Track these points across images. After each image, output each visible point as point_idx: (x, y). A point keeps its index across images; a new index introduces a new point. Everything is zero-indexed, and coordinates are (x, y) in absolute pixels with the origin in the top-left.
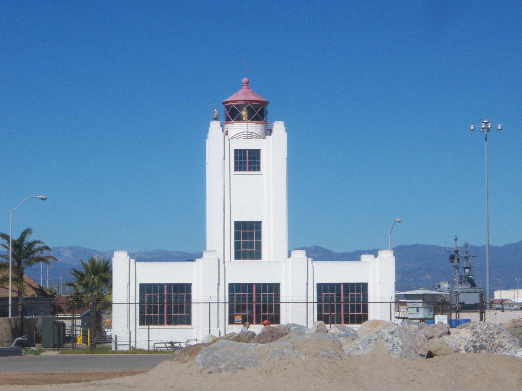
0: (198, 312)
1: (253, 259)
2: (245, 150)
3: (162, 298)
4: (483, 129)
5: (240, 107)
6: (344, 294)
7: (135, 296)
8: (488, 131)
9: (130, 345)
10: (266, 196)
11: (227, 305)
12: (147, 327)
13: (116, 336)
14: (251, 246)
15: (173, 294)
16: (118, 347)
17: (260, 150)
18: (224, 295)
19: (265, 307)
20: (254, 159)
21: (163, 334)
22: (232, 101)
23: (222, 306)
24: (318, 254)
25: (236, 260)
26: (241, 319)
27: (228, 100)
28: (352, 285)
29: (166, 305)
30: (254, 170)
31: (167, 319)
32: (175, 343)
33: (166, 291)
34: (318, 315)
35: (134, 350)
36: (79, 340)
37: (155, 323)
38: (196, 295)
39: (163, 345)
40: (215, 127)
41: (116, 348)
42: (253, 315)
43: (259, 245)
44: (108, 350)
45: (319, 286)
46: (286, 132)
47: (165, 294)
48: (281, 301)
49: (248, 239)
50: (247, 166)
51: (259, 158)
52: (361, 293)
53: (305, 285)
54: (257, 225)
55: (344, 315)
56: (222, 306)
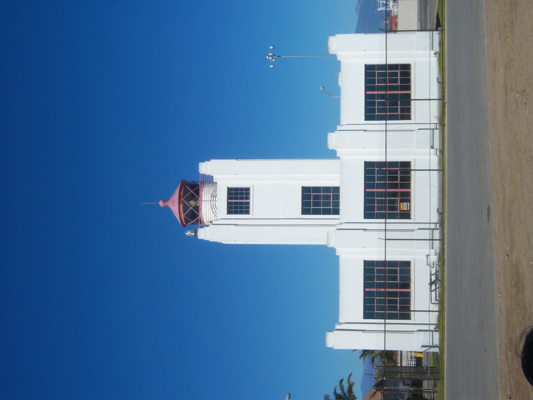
0: (396, 254)
1: (339, 209)
2: (229, 204)
3: (380, 294)
4: (272, 59)
5: (185, 208)
6: (378, 91)
7: (377, 324)
8: (274, 55)
9: (432, 331)
10: (275, 183)
11: (388, 221)
12: (412, 313)
13: (423, 346)
14: (328, 197)
15: (376, 281)
16: (434, 344)
17: (228, 188)
18: (377, 224)
19: (391, 179)
20: (237, 194)
21: (422, 295)
22: (180, 216)
23: (389, 227)
24: (332, 120)
25: (340, 213)
26: (405, 203)
27: (179, 221)
28: (366, 179)
29: (387, 290)
30: (248, 194)
31: (403, 288)
32: (431, 279)
33: (372, 290)
34: (401, 119)
35: (439, 327)
36: (420, 356)
37: (408, 302)
38: (377, 256)
39: (433, 293)
40: (203, 234)
41: (436, 346)
42: (401, 192)
43: (327, 189)
44: (438, 358)
45: (367, 118)
46: (209, 160)
47: (375, 290)
48: (384, 160)
49: (319, 201)
50: (244, 201)
51: (236, 189)
52: (377, 72)
53: (366, 133)
54: (306, 190)
55: (401, 90)
56: (389, 227)
